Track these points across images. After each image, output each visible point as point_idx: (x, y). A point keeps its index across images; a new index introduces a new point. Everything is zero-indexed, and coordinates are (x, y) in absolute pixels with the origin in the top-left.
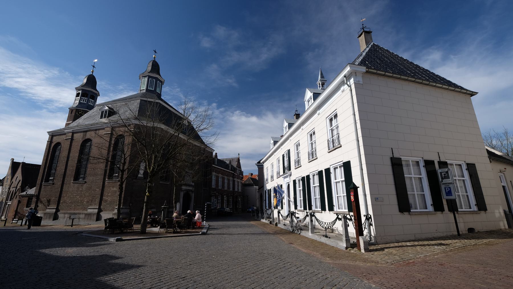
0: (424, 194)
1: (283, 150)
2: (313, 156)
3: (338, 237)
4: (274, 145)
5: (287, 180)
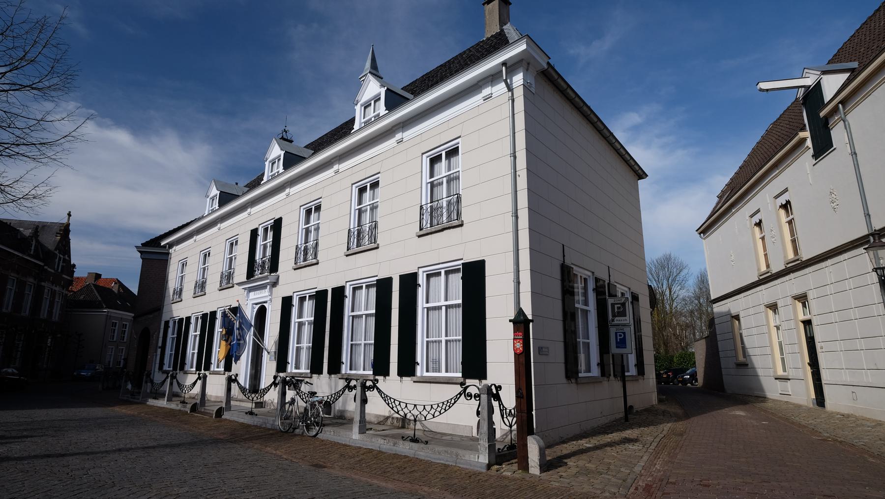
0: (588, 343)
1: (260, 215)
3: (469, 443)
4: (222, 204)
5: (261, 296)
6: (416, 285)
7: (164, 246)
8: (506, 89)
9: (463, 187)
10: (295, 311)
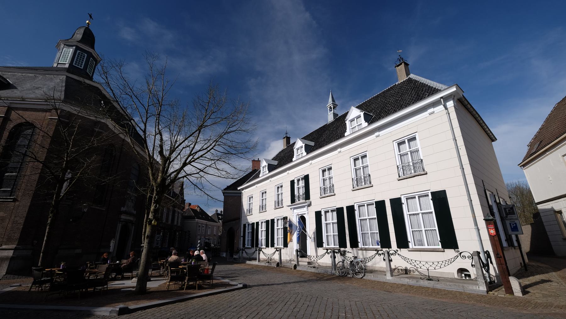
1: (296, 173)
2: (263, 208)
6: (274, 222)
7: (240, 190)
8: (444, 109)
9: (334, 181)
10: (276, 224)
